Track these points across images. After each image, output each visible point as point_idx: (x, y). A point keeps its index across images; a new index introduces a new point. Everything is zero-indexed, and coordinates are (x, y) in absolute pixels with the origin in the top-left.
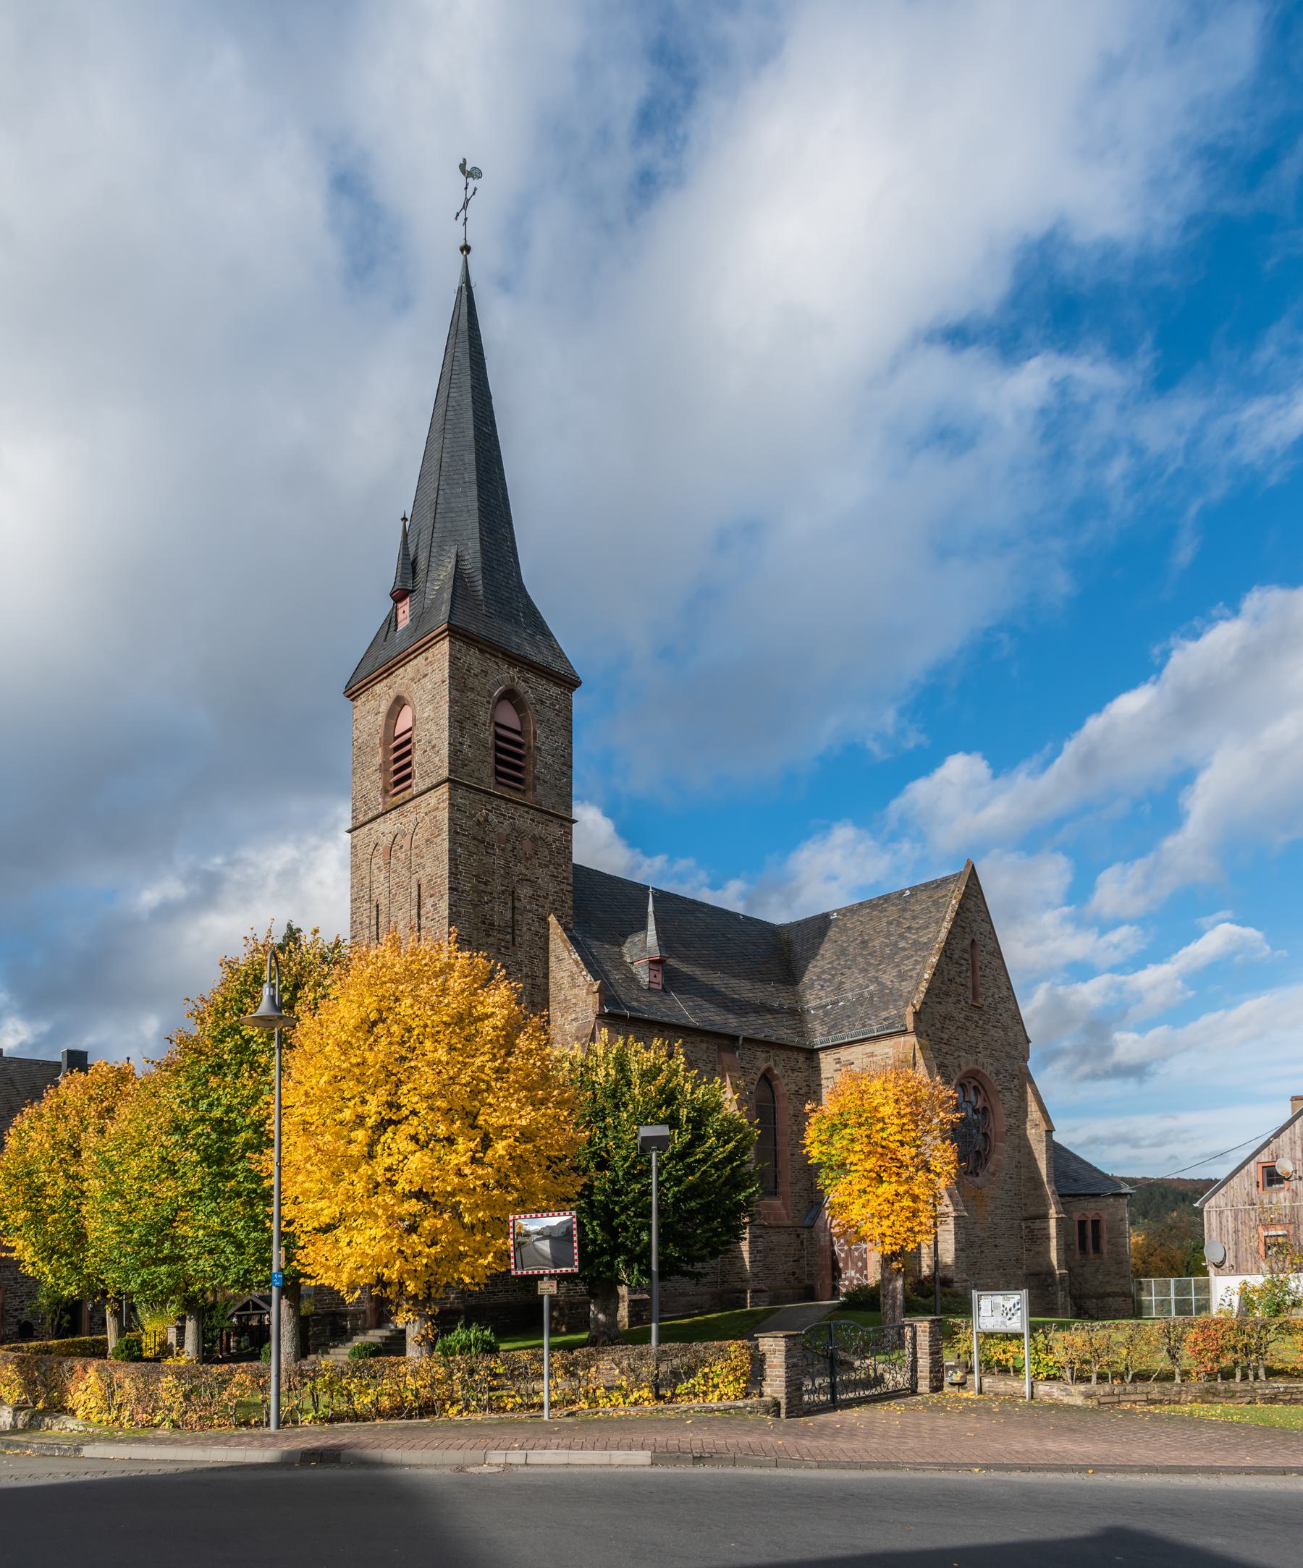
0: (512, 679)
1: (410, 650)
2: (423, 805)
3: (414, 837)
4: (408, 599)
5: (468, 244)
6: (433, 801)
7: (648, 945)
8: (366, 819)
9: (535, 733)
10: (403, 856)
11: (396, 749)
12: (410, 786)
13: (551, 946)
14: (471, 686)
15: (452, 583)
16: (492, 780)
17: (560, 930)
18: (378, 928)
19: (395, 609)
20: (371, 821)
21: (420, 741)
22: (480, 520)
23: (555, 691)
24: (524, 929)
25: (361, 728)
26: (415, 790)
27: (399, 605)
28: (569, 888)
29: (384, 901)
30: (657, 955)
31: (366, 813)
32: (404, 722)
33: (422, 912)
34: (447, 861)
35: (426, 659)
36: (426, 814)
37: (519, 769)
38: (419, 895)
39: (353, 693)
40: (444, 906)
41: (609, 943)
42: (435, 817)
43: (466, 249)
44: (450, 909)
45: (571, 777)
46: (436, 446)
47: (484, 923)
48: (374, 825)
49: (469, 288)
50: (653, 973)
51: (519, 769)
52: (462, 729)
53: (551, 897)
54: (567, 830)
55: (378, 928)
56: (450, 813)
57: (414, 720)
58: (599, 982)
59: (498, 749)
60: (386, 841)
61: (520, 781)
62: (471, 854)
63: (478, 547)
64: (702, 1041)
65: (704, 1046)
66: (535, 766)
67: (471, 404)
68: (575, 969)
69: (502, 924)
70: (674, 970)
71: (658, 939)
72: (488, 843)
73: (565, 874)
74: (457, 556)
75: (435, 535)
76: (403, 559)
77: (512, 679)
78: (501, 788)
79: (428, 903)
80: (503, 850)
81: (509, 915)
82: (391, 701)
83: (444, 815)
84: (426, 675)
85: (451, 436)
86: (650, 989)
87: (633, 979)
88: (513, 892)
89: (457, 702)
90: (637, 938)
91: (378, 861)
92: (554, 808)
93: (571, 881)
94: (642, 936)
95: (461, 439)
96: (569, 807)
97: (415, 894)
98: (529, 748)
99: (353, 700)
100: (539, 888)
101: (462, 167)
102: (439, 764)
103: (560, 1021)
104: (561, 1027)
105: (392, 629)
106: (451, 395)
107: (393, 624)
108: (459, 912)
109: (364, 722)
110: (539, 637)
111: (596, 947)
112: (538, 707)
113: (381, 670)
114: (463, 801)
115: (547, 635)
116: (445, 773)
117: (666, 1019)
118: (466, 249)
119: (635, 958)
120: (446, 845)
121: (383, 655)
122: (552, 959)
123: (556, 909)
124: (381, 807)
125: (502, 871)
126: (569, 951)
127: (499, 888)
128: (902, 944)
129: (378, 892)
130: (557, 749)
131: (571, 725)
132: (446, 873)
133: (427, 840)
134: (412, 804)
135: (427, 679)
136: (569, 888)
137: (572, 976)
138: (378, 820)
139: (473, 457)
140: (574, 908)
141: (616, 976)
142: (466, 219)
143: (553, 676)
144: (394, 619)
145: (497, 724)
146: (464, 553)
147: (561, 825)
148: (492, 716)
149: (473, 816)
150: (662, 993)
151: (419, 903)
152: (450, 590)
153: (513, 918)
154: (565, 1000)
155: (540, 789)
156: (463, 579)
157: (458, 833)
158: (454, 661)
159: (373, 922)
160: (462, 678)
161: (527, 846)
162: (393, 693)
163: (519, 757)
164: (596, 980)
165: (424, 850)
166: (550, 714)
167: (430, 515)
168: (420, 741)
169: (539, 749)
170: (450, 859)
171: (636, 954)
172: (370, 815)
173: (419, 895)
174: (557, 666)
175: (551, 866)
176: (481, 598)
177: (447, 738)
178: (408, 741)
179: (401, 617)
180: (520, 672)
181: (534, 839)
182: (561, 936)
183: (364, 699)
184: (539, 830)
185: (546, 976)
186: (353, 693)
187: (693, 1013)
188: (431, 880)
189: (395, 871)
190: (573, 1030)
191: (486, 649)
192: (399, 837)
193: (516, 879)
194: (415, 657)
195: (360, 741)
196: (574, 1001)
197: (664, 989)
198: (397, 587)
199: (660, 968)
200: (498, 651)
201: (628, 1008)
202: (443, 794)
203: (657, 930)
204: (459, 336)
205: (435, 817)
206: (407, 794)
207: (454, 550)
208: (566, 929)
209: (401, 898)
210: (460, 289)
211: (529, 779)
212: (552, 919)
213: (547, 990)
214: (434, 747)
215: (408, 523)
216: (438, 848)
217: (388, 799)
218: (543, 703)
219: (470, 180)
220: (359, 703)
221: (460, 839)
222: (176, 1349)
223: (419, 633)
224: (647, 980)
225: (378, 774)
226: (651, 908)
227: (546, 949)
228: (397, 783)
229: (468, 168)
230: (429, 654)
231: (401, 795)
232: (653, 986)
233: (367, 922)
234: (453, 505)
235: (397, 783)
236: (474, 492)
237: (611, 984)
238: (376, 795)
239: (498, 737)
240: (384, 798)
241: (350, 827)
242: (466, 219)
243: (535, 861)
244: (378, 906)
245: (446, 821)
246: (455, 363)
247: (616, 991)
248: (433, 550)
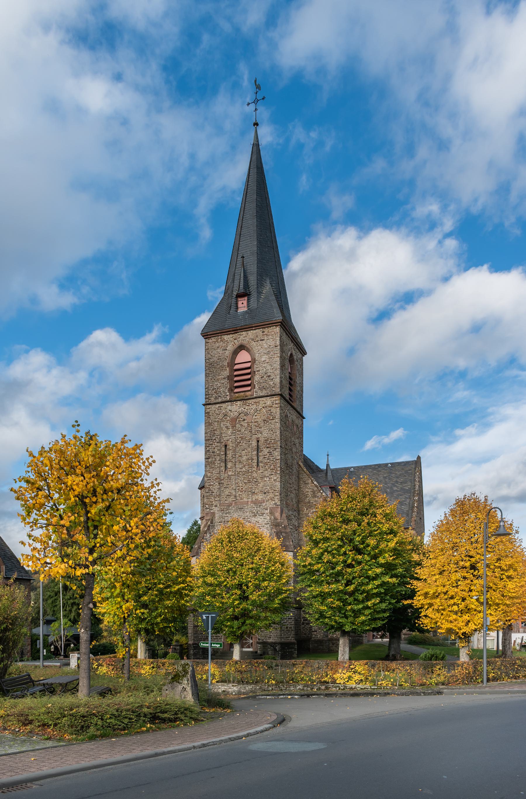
20: (221, 403)
31: (216, 398)
35: (263, 332)
39: (208, 335)
68: (315, 489)
128: (395, 488)
137: (314, 492)
154: (309, 502)
162: (237, 343)
186: (208, 335)
202: (276, 400)
222: (435, 656)
230: (266, 330)
241: (204, 403)
244: (226, 446)
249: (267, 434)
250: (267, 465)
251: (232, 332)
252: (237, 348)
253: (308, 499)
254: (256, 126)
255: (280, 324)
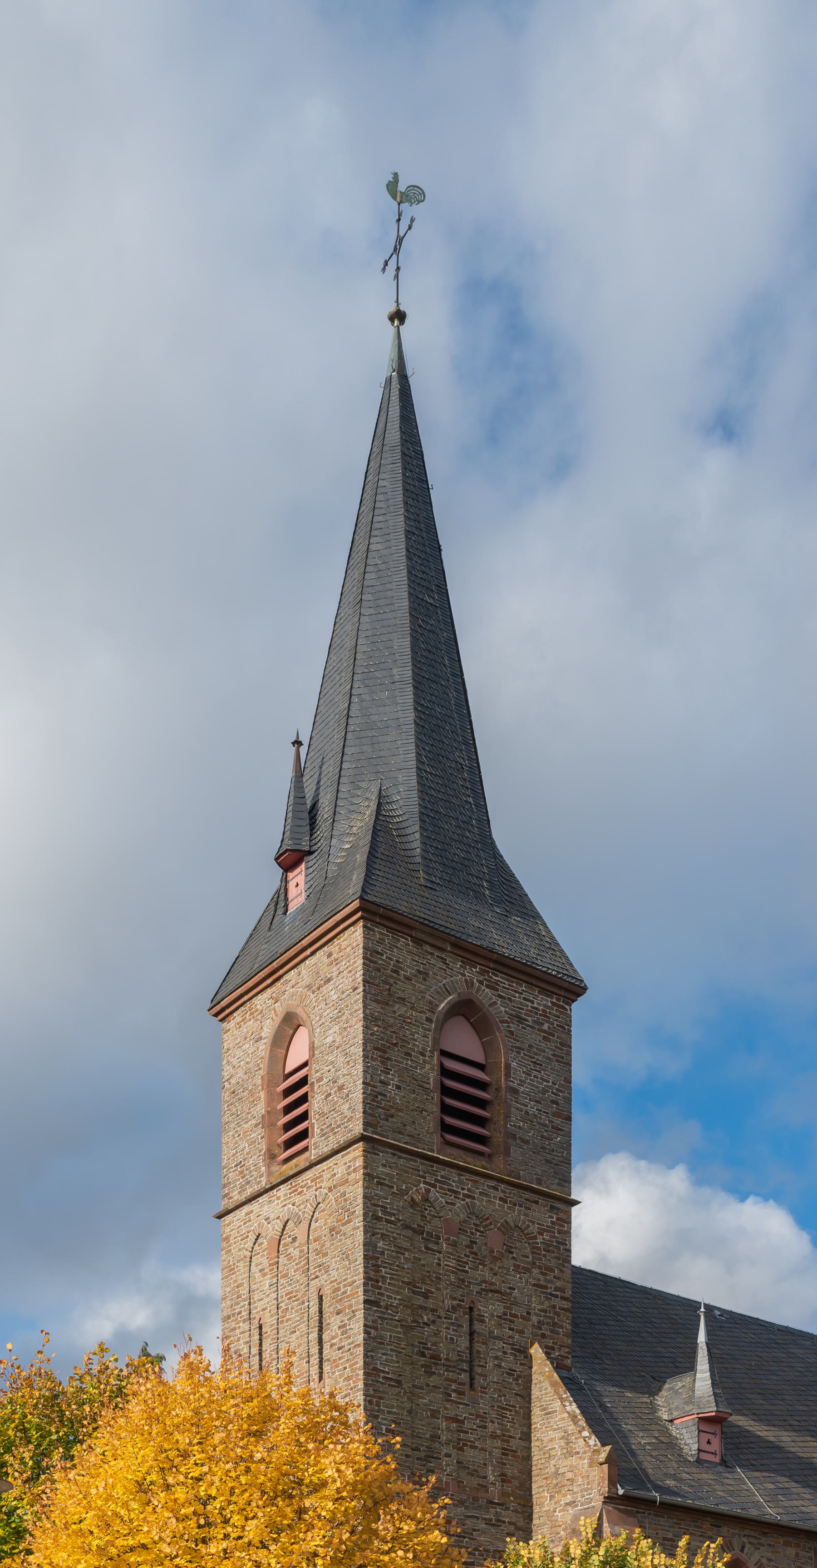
0: (470, 984)
1: (305, 942)
2: (326, 1175)
3: (313, 1225)
4: (303, 866)
5: (402, 308)
6: (341, 1171)
7: (698, 1393)
8: (243, 1198)
9: (508, 1066)
10: (296, 1253)
11: (288, 1092)
12: (306, 1149)
13: (535, 1392)
14: (401, 994)
15: (369, 837)
16: (436, 1139)
17: (548, 1368)
18: (261, 1360)
19: (285, 881)
21: (320, 1079)
22: (418, 739)
23: (542, 1001)
24: (490, 1365)
25: (235, 1061)
26: (313, 1154)
27: (290, 875)
28: (566, 1305)
29: (269, 1321)
30: (711, 1409)
31: (243, 1189)
32: (297, 1054)
33: (325, 1337)
34: (361, 1260)
35: (330, 955)
36: (330, 1190)
37: (481, 1121)
38: (321, 1312)
40: (357, 1327)
41: (633, 1389)
42: (344, 1194)
43: (399, 316)
44: (366, 1332)
45: (569, 1134)
46: (349, 627)
47: (423, 1355)
48: (254, 1206)
49: (403, 378)
50: (705, 1437)
51: (481, 1121)
52: (385, 1060)
53: (534, 1319)
54: (561, 1215)
55: (261, 1360)
56: (365, 1188)
57: (312, 1048)
58: (608, 1448)
59: (446, 1091)
60: (272, 1230)
61: (481, 1140)
62: (400, 1250)
63: (414, 782)
64: (786, 1544)
65: (791, 1551)
66: (507, 1117)
67: (404, 559)
68: (571, 1428)
69: (453, 1356)
70: (743, 1433)
71: (714, 1384)
72: (430, 1234)
73: (559, 1284)
74: (380, 796)
75: (344, 766)
76: (295, 803)
77: (470, 984)
78: (449, 1150)
79: (333, 1322)
80: (454, 1245)
81: (464, 1343)
82: (278, 1020)
83: (356, 1191)
84: (329, 980)
85: (371, 611)
86: (699, 1461)
87: (671, 1445)
88: (471, 1309)
89: (376, 1019)
90: (678, 1384)
91: (262, 1260)
92: (539, 1182)
93: (568, 1293)
94: (687, 1379)
95: (389, 615)
96: (566, 1181)
97: (314, 1309)
98: (498, 1090)
99: (222, 1020)
100: (515, 1303)
101: (392, 187)
102: (348, 1114)
103: (548, 1505)
104: (550, 1514)
105: (280, 911)
106: (372, 547)
107: (281, 904)
108: (382, 1337)
109: (239, 1053)
110: (514, 919)
111: (610, 1394)
112: (513, 1027)
113: (262, 975)
114: (387, 1170)
115: (529, 913)
116: (357, 1127)
117: (723, 1508)
118: (399, 316)
119: (676, 1414)
120: (360, 1237)
121: (265, 952)
122: (536, 1412)
123: (543, 1336)
124: (264, 1180)
125: (452, 1278)
126: (562, 1400)
127: (448, 1303)
129: (260, 1305)
130: (544, 1092)
131: (569, 1054)
132: (360, 1279)
133: (332, 1229)
134: (309, 1174)
135: (330, 986)
136: (566, 1305)
137: (566, 1438)
138: (261, 1199)
139: (407, 642)
140: (574, 1334)
141: (640, 1440)
142: (398, 269)
143: (538, 979)
144: (282, 897)
145: (444, 1053)
146: (391, 791)
147: (552, 1207)
148: (436, 1041)
149: (402, 1193)
150: (720, 1469)
151: (321, 1322)
152: (366, 849)
153: (471, 1347)
154: (556, 1474)
155: (516, 1153)
156: (388, 832)
157: (378, 1219)
158: (371, 957)
159: (255, 1350)
160: (385, 982)
161: (495, 1239)
162: (280, 1009)
163: (482, 1103)
164: (604, 1445)
165: (328, 1244)
166: (534, 1038)
167: (338, 736)
168: (320, 1079)
169: (515, 1091)
170: (366, 1257)
171: (677, 1408)
172: (249, 1192)
173: (321, 1312)
174: (545, 963)
175: (535, 1271)
176: (419, 859)
177: (361, 1075)
178: (304, 1081)
179: (292, 892)
180: (482, 972)
181: (506, 1228)
182: (550, 1377)
183: (238, 1019)
184: (515, 1216)
185: (527, 1437)
187: (772, 1499)
188: (338, 1289)
189: (286, 1275)
190: (568, 1519)
191: (423, 937)
192: (290, 1225)
193: (475, 1289)
194: (313, 953)
195: (233, 1081)
196: (569, 1475)
197: (724, 1463)
198: (284, 848)
199: (717, 1429)
200: (445, 940)
201: (658, 1488)
203: (712, 1370)
204: (384, 455)
205: (344, 1194)
206: (301, 1161)
207: (375, 789)
208: (558, 1367)
209: (293, 1315)
210: (389, 381)
211: (498, 1138)
212: (536, 1351)
213: (528, 1458)
214: (341, 1088)
215: (303, 750)
216: (349, 1241)
217: (275, 1168)
218: (521, 1020)
219: (405, 206)
220: (231, 1024)
221: (381, 1227)
223: (317, 918)
224: (696, 1447)
225: (260, 1131)
226: (702, 1337)
227: (526, 1397)
228: (289, 1143)
229: (402, 187)
230: (333, 947)
231: (295, 1161)
232: (703, 1456)
233: (246, 1350)
234: (375, 718)
235: (289, 1143)
236: (408, 696)
237: (633, 1453)
238: (256, 1161)
239: (445, 1072)
240: (268, 1167)
242: (398, 269)
243: (509, 1263)
244: (260, 1327)
245: (360, 1200)
246: (379, 497)
247: (640, 1463)
248: (343, 788)
249: (338, 1269)
250: (337, 1366)
251: (269, 981)
252: (279, 1027)
253: (553, 1462)
254: (396, 322)
255: (359, 914)
